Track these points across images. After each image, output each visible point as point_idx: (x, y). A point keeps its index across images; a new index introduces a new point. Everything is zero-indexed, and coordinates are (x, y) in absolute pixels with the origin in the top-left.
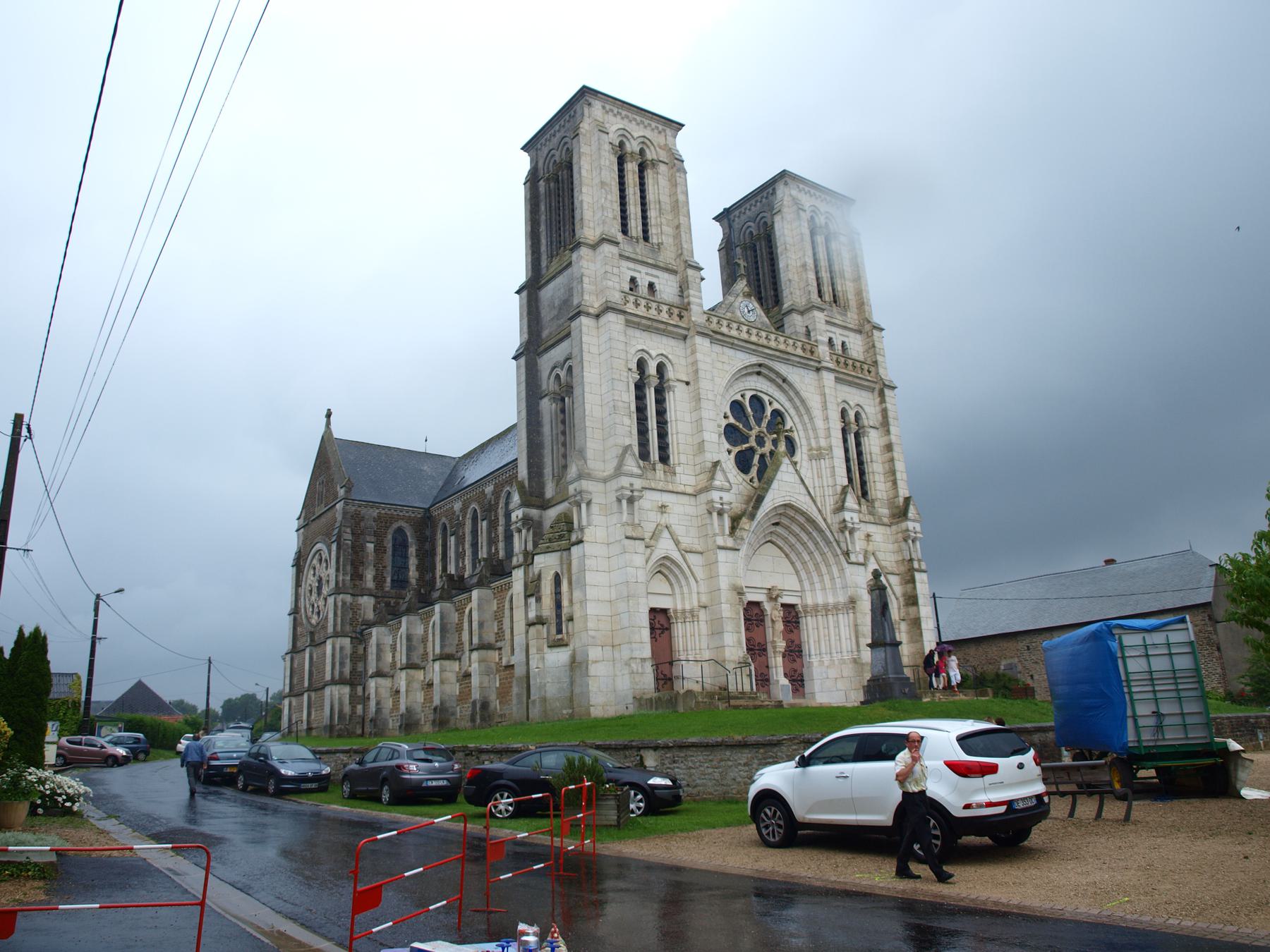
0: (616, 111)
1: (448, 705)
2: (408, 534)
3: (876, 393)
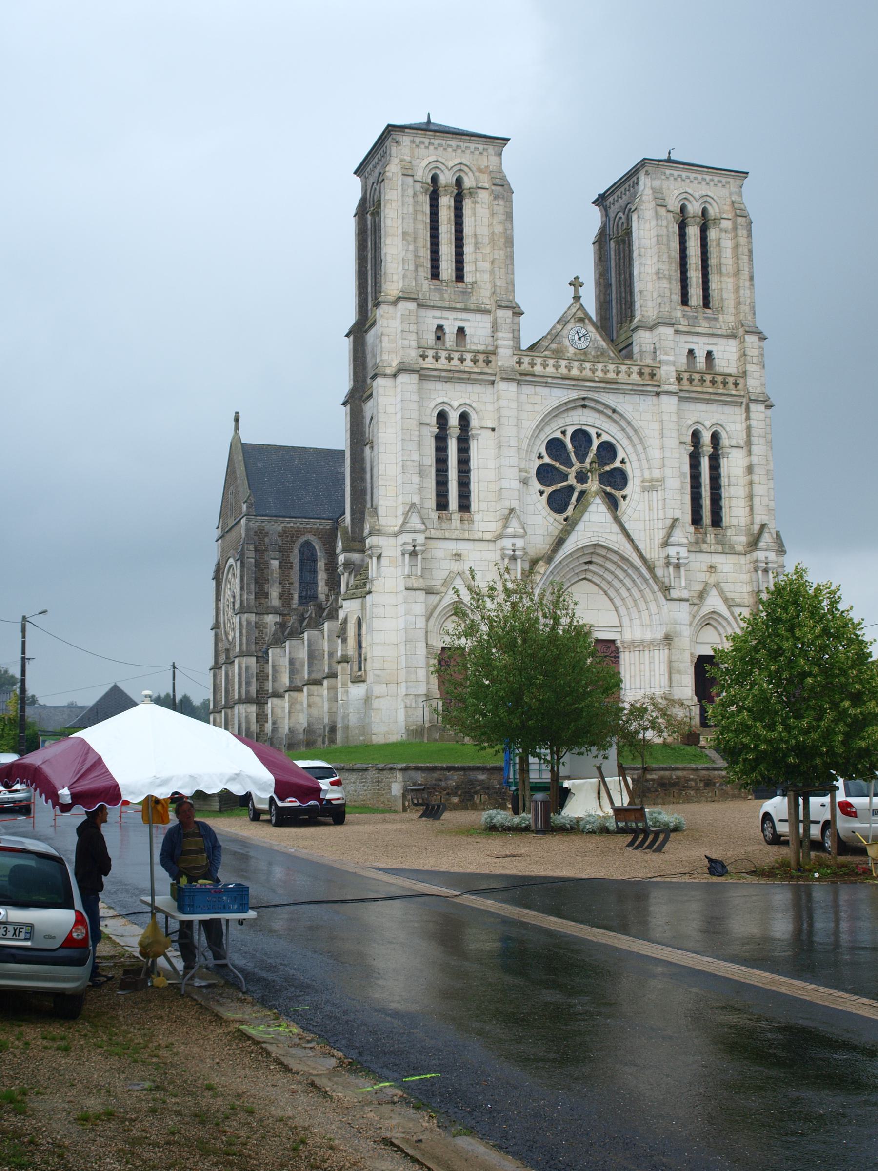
0: (427, 141)
1: (315, 727)
2: (317, 547)
3: (744, 406)
